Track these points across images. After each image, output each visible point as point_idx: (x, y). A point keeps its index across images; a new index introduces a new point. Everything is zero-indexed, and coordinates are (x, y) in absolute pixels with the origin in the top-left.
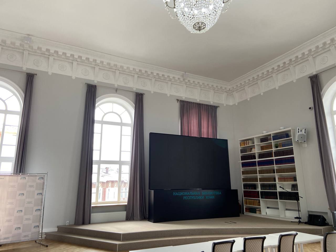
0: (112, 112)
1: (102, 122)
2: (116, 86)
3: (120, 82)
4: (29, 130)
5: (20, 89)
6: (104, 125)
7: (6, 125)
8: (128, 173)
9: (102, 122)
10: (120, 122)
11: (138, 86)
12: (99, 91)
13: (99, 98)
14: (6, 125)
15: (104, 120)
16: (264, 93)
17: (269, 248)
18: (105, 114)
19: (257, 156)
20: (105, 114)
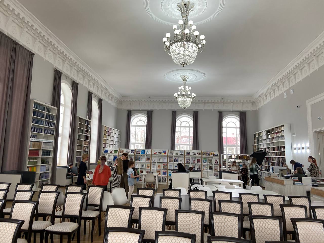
0: (231, 122)
1: (226, 127)
2: (232, 110)
3: (231, 108)
4: (76, 126)
5: (238, 116)
6: (227, 129)
7: (226, 129)
8: (131, 139)
9: (226, 127)
10: (189, 126)
11: (241, 108)
12: (223, 114)
13: (224, 117)
14: (226, 129)
15: (227, 126)
16: (159, 109)
17: (49, 235)
18: (136, 125)
19: (162, 152)
20: (136, 125)
